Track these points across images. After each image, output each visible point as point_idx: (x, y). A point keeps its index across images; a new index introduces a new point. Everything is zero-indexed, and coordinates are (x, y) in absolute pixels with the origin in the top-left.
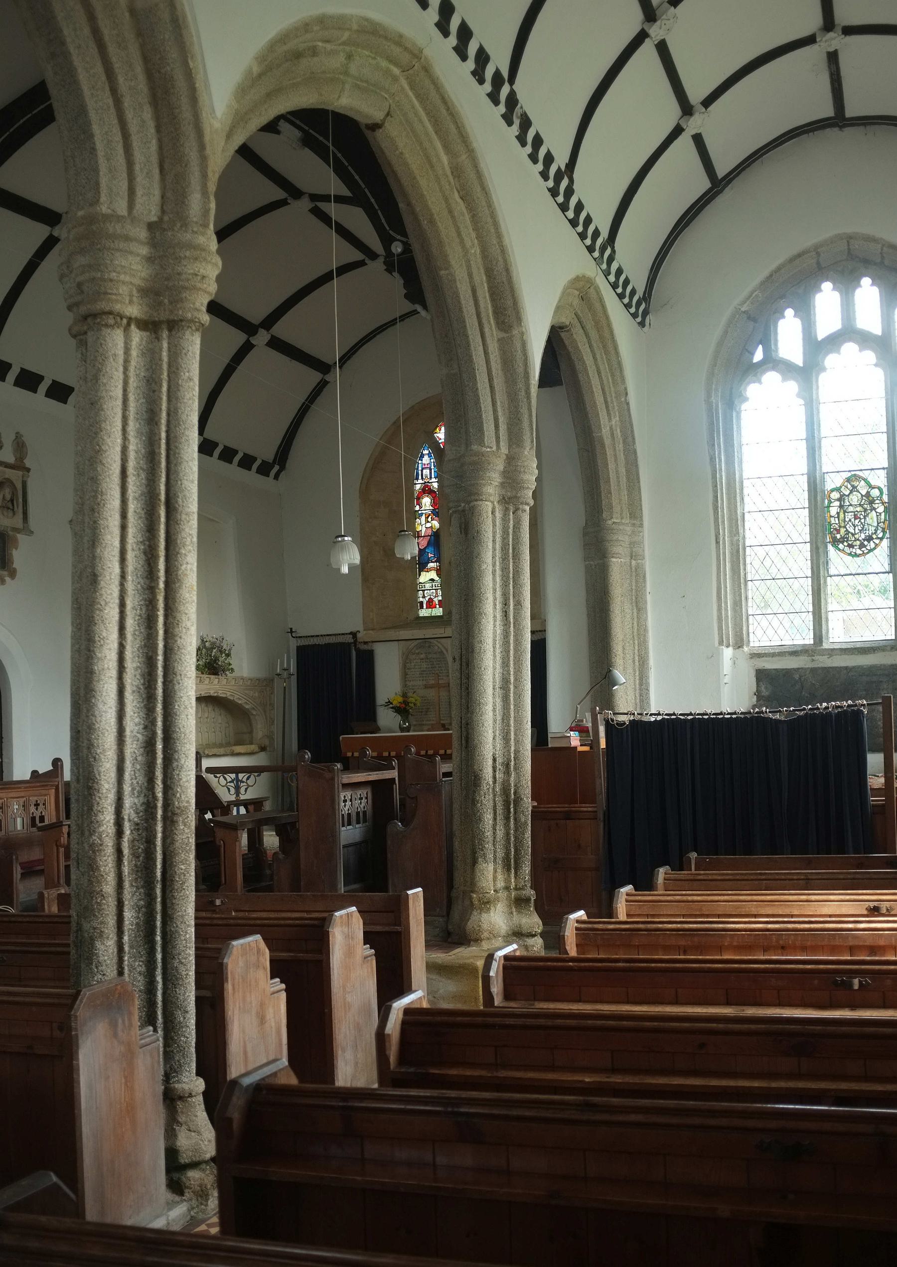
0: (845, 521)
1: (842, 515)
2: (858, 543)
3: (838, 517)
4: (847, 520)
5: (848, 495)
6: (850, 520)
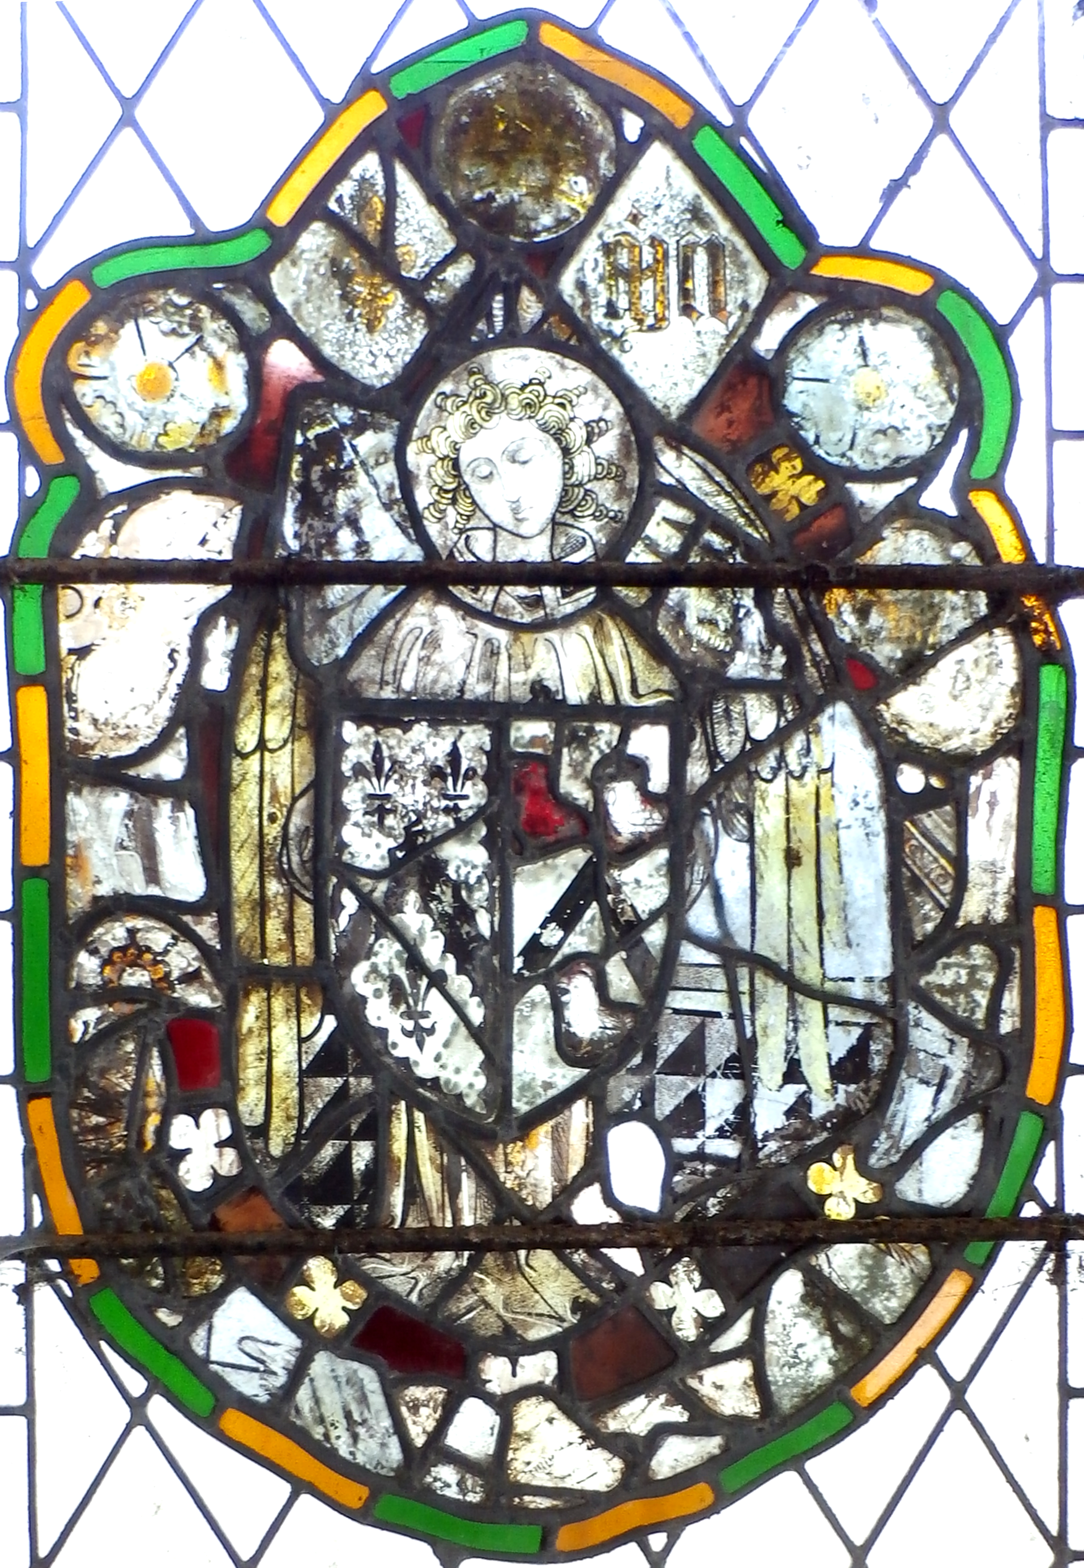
0: (319, 866)
1: (271, 765)
2: (550, 1288)
3: (208, 791)
4: (367, 847)
5: (400, 402)
6: (418, 861)
